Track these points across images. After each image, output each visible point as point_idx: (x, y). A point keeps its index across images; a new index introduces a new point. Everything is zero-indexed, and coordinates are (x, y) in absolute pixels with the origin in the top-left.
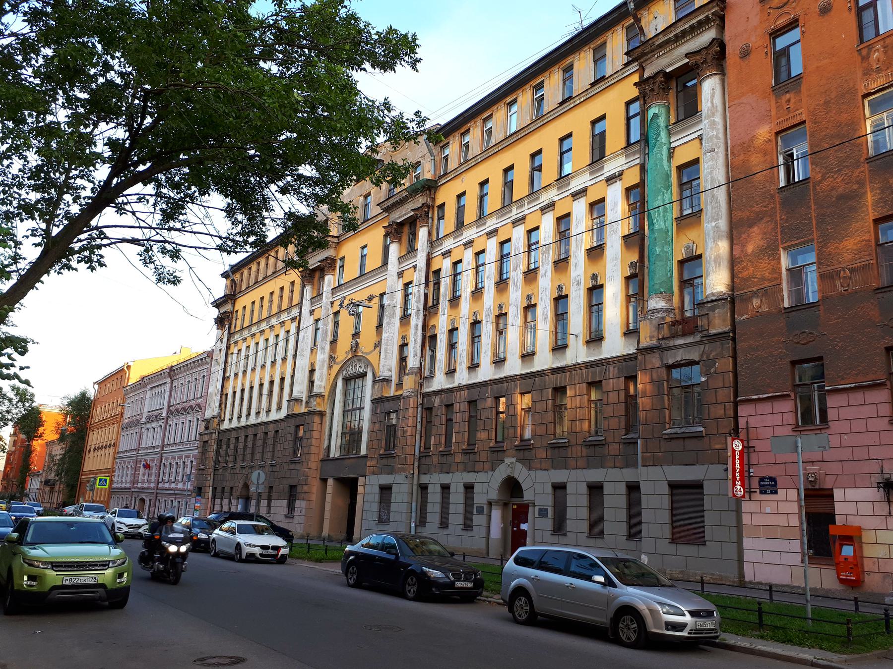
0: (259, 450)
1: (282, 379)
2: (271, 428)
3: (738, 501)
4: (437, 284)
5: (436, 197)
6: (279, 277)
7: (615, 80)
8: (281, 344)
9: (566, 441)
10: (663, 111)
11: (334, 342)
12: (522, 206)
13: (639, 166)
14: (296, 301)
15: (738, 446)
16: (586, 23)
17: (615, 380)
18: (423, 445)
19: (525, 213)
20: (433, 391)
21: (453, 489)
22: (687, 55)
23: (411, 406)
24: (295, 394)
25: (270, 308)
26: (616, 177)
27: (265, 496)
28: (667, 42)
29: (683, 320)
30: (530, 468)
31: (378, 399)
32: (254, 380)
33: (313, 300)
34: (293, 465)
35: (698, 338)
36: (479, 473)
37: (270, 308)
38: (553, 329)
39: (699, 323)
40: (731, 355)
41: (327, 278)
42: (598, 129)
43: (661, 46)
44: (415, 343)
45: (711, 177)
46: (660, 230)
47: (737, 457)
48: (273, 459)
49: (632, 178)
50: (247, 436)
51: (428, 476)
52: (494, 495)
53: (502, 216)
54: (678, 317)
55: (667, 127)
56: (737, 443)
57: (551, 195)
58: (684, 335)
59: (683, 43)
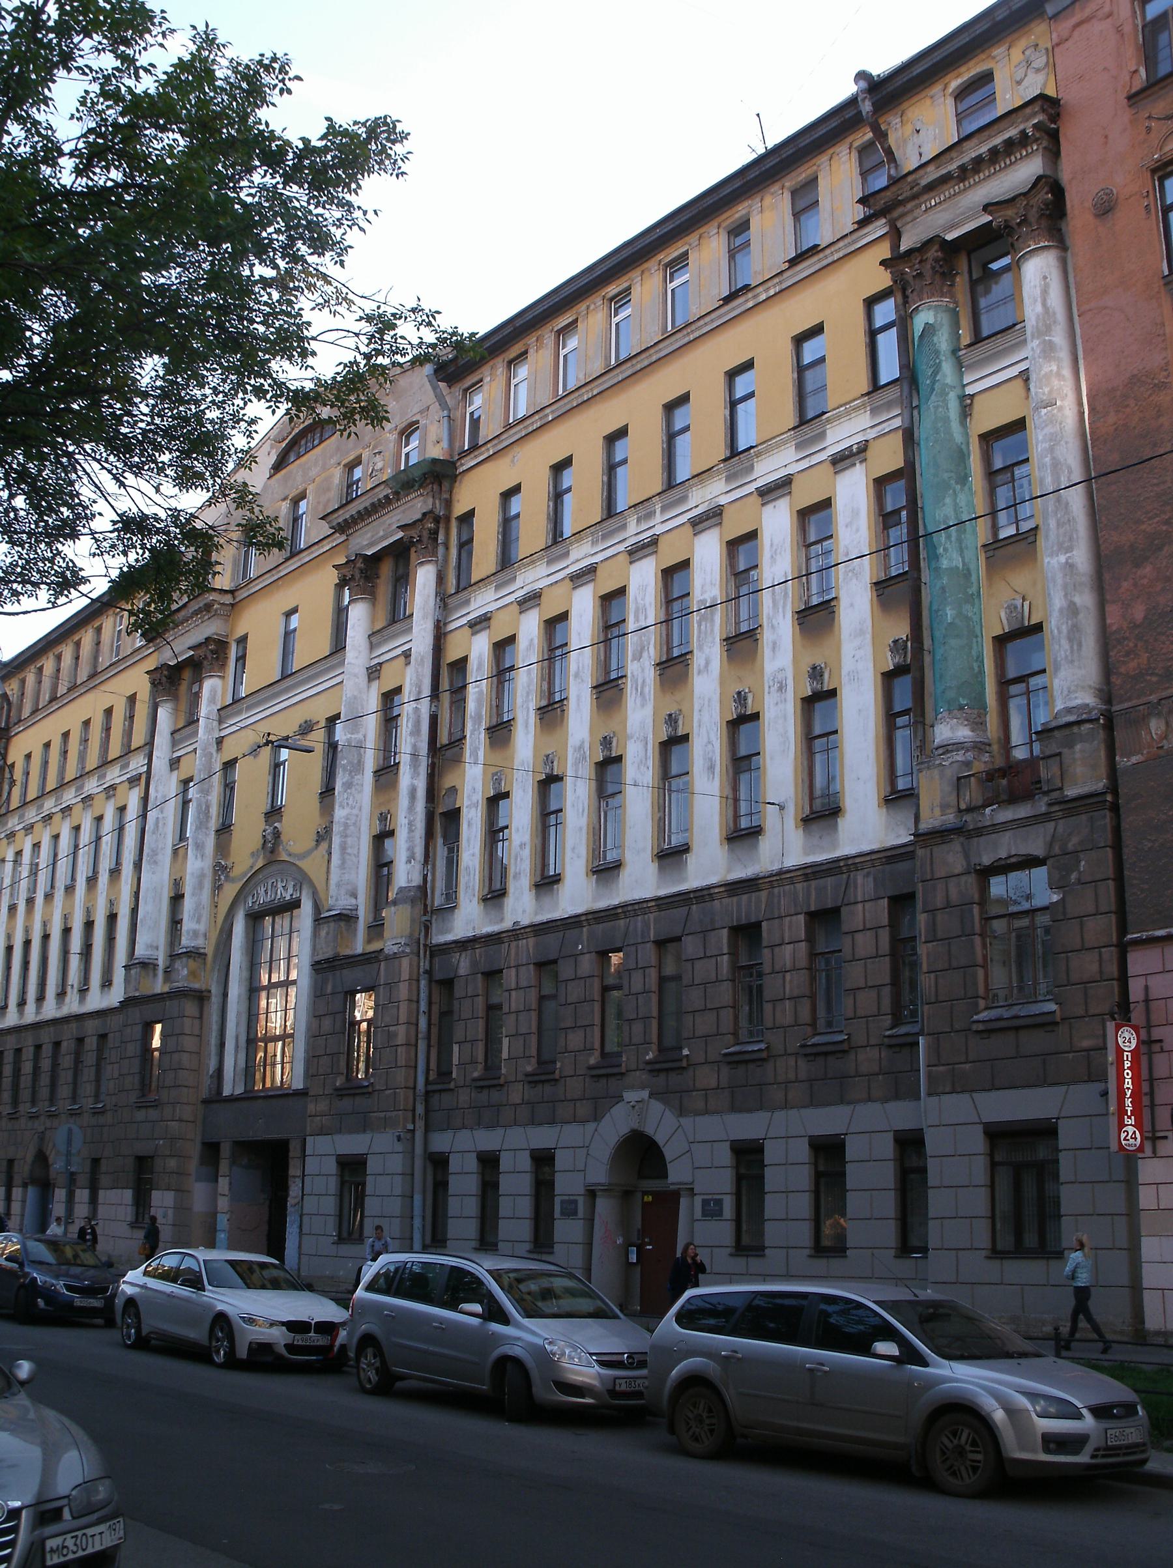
0: (65, 1077)
1: (112, 918)
2: (91, 1026)
3: (1130, 1159)
4: (459, 692)
5: (455, 497)
6: (103, 688)
7: (841, 254)
8: (107, 842)
9: (763, 1046)
10: (944, 319)
11: (225, 829)
12: (650, 515)
13: (900, 433)
14: (138, 739)
15: (1127, 1040)
16: (775, 138)
17: (868, 905)
18: (433, 1065)
19: (658, 530)
20: (455, 942)
21: (505, 1163)
22: (987, 208)
23: (405, 975)
24: (140, 951)
25: (82, 757)
26: (852, 455)
27: (83, 1179)
28: (945, 179)
29: (1010, 767)
30: (682, 1112)
31: (327, 961)
32: (50, 920)
33: (177, 736)
34: (143, 1111)
35: (1041, 806)
36: (566, 1128)
37: (82, 757)
38: (728, 791)
39: (1043, 774)
40: (1109, 843)
41: (208, 685)
42: (810, 352)
43: (931, 187)
44: (411, 831)
45: (1053, 458)
46: (953, 570)
47: (1127, 1064)
48: (97, 1097)
49: (889, 457)
50: (38, 1047)
51: (448, 1135)
52: (599, 1174)
53: (605, 537)
54: (999, 762)
55: (955, 352)
56: (1127, 1035)
57: (714, 492)
58: (1013, 799)
59: (975, 183)
